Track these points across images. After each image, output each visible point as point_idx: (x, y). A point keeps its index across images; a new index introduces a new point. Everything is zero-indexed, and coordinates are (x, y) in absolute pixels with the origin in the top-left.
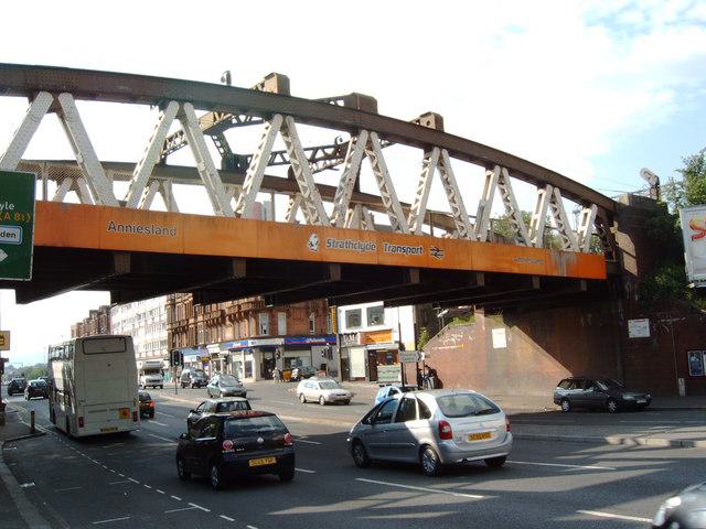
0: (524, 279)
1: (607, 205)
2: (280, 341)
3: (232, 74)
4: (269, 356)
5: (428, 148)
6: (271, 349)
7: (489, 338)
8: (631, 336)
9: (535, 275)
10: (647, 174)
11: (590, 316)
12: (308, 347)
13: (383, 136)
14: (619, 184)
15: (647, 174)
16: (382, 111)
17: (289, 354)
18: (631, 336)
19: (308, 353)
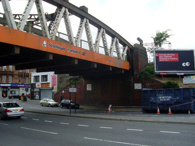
0: (71, 59)
1: (131, 47)
2: (9, 85)
3: (142, 38)
4: (5, 90)
5: (82, 18)
6: (6, 87)
7: (86, 87)
8: (135, 88)
9: (51, 53)
10: (139, 39)
11: (121, 81)
12: (18, 88)
13: (70, 11)
14: (133, 41)
15: (139, 39)
16: (89, 12)
17: (11, 90)
18: (135, 88)
19: (18, 90)
